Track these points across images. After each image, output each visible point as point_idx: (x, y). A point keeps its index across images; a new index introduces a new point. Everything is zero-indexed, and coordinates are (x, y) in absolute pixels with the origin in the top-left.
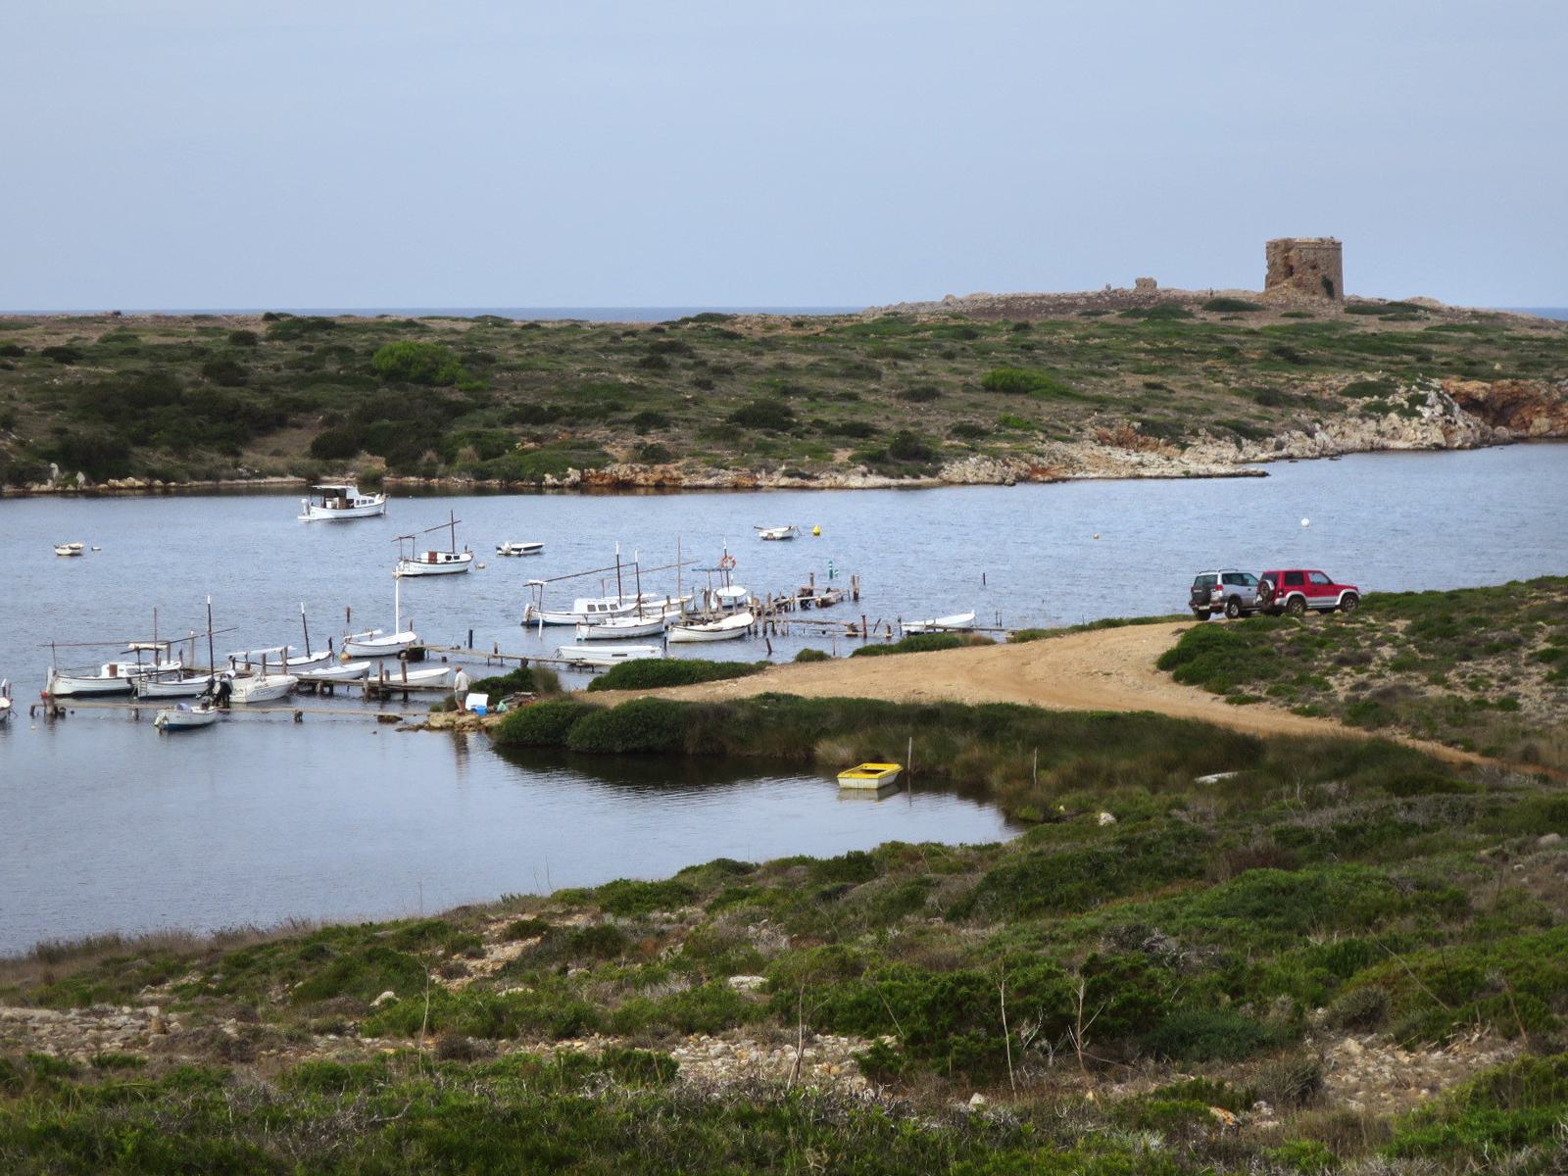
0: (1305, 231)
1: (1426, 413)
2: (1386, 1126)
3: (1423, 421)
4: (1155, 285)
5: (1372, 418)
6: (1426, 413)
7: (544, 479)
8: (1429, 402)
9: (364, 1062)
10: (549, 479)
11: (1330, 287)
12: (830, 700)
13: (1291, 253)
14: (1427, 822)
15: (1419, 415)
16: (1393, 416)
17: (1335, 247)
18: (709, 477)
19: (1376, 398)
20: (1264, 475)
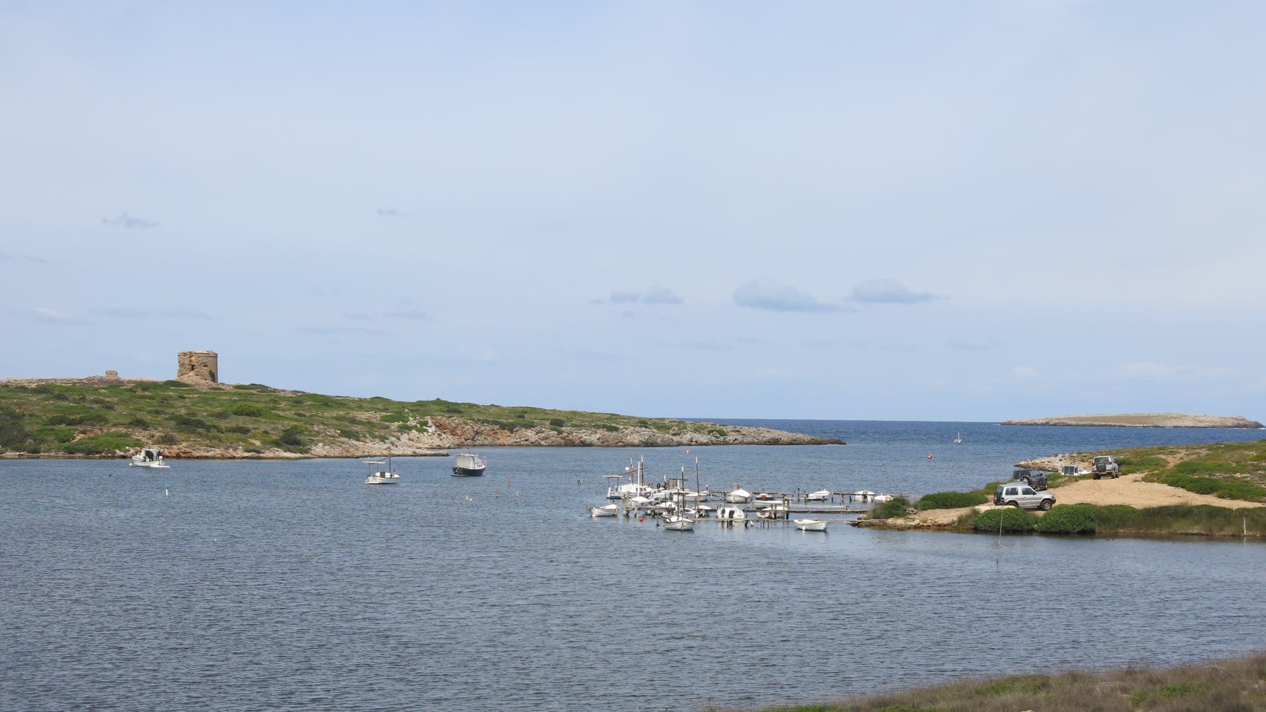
0: (201, 348)
1: (430, 430)
2: (1037, 701)
3: (429, 434)
4: (117, 374)
5: (405, 432)
6: (430, 430)
7: (115, 453)
8: (429, 425)
9: (782, 704)
10: (119, 453)
11: (213, 376)
12: (942, 508)
13: (193, 358)
14: (8, 671)
15: (426, 431)
16: (414, 431)
17: (216, 356)
18: (208, 452)
19: (401, 422)
20: (447, 455)
